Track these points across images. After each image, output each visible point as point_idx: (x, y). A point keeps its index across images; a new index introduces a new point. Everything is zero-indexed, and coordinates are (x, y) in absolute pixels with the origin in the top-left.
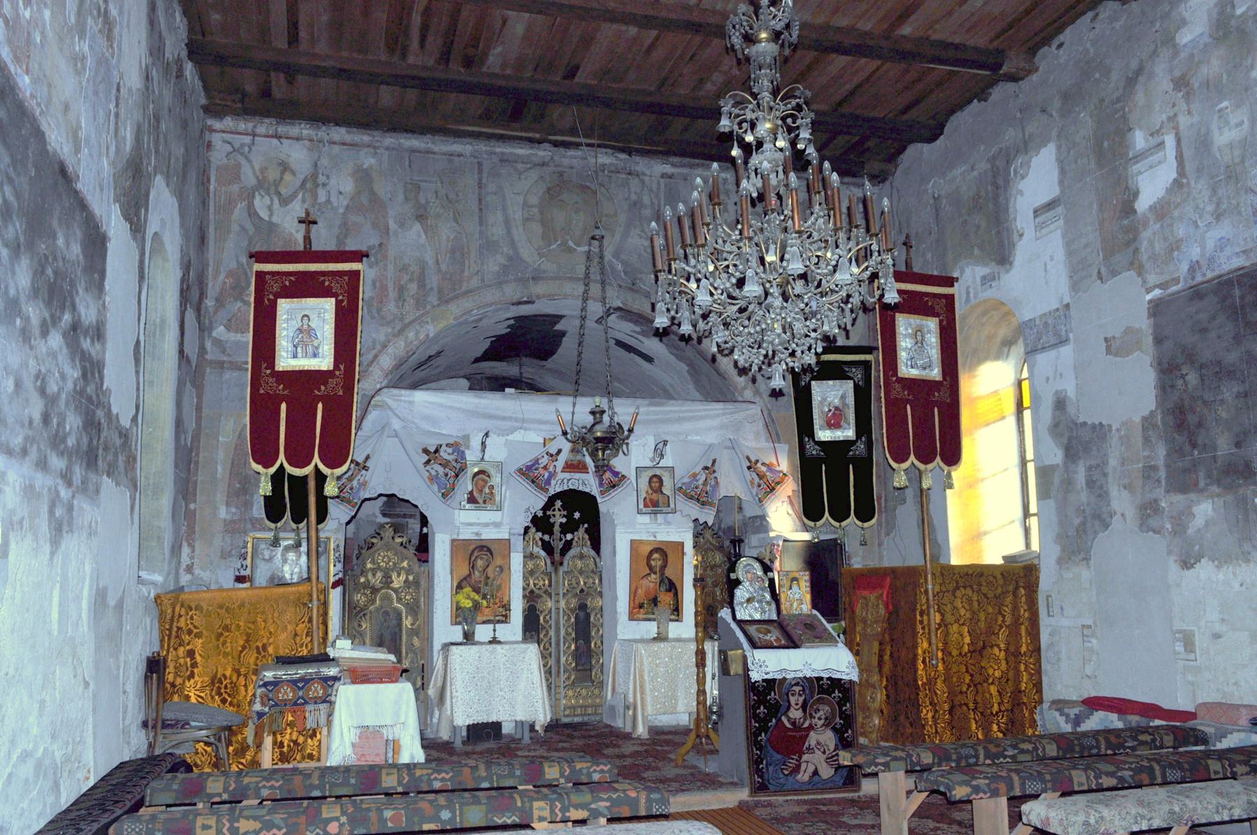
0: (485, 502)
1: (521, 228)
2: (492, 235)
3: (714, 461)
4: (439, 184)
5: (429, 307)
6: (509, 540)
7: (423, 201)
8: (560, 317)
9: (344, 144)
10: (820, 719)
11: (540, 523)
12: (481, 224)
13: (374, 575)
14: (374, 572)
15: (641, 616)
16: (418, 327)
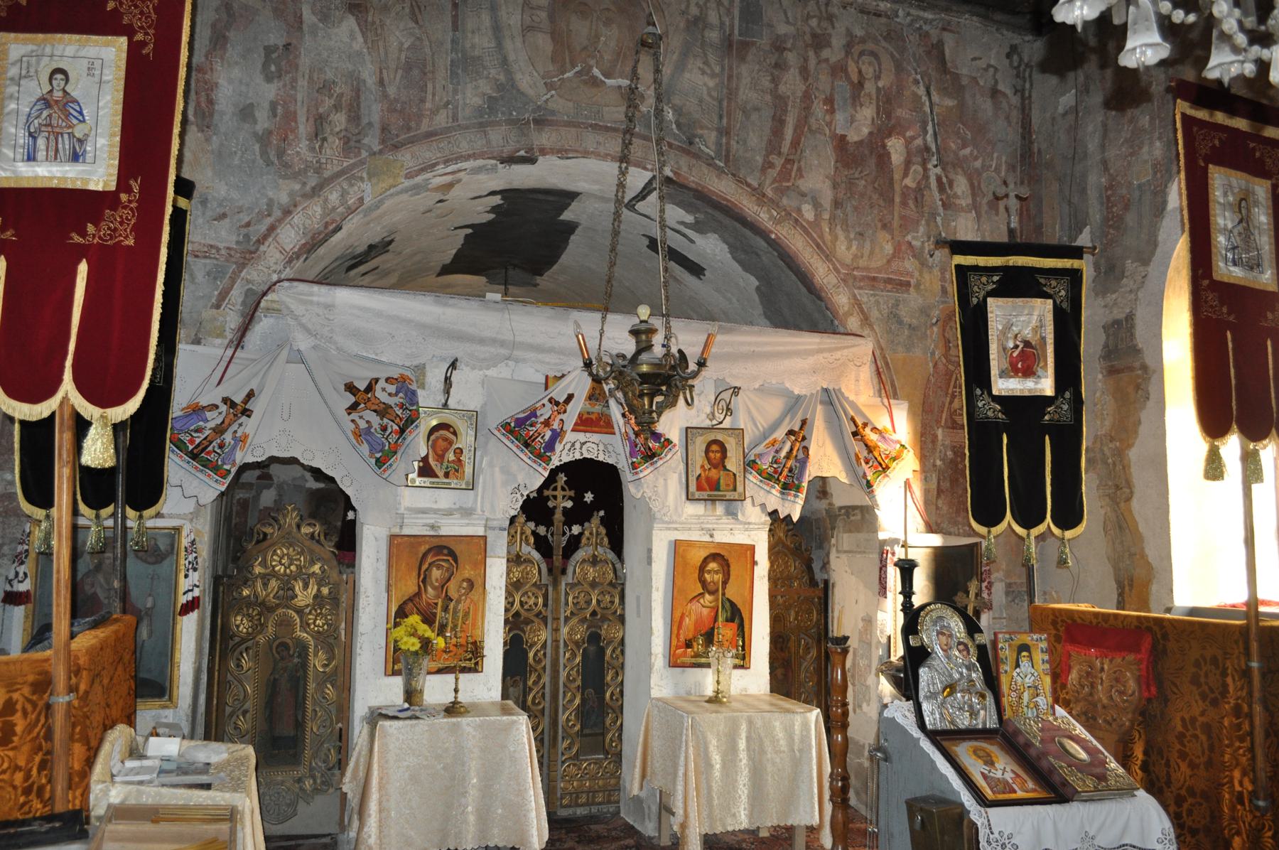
0: (447, 475)
1: (519, 43)
2: (473, 47)
5: (364, 154)
6: (485, 537)
8: (571, 196)
11: (535, 508)
12: (455, 27)
13: (265, 585)
14: (265, 579)
15: (688, 660)
16: (345, 186)
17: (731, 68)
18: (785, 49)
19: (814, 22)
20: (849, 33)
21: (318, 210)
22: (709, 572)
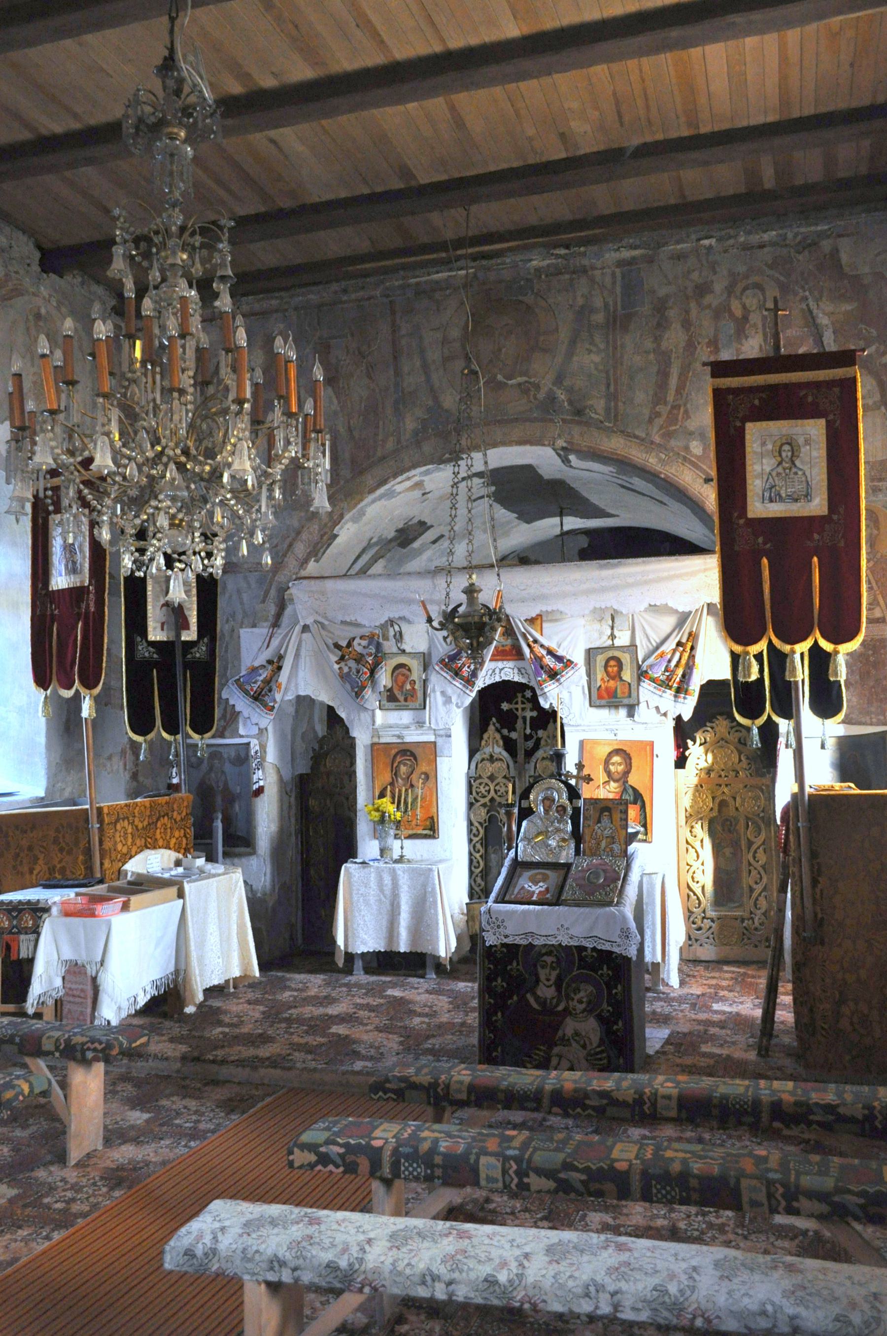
0: (406, 700)
4: (350, 338)
5: (342, 482)
6: (435, 743)
17: (615, 341)
18: (666, 309)
19: (695, 276)
20: (732, 274)
21: (316, 527)
22: (613, 764)
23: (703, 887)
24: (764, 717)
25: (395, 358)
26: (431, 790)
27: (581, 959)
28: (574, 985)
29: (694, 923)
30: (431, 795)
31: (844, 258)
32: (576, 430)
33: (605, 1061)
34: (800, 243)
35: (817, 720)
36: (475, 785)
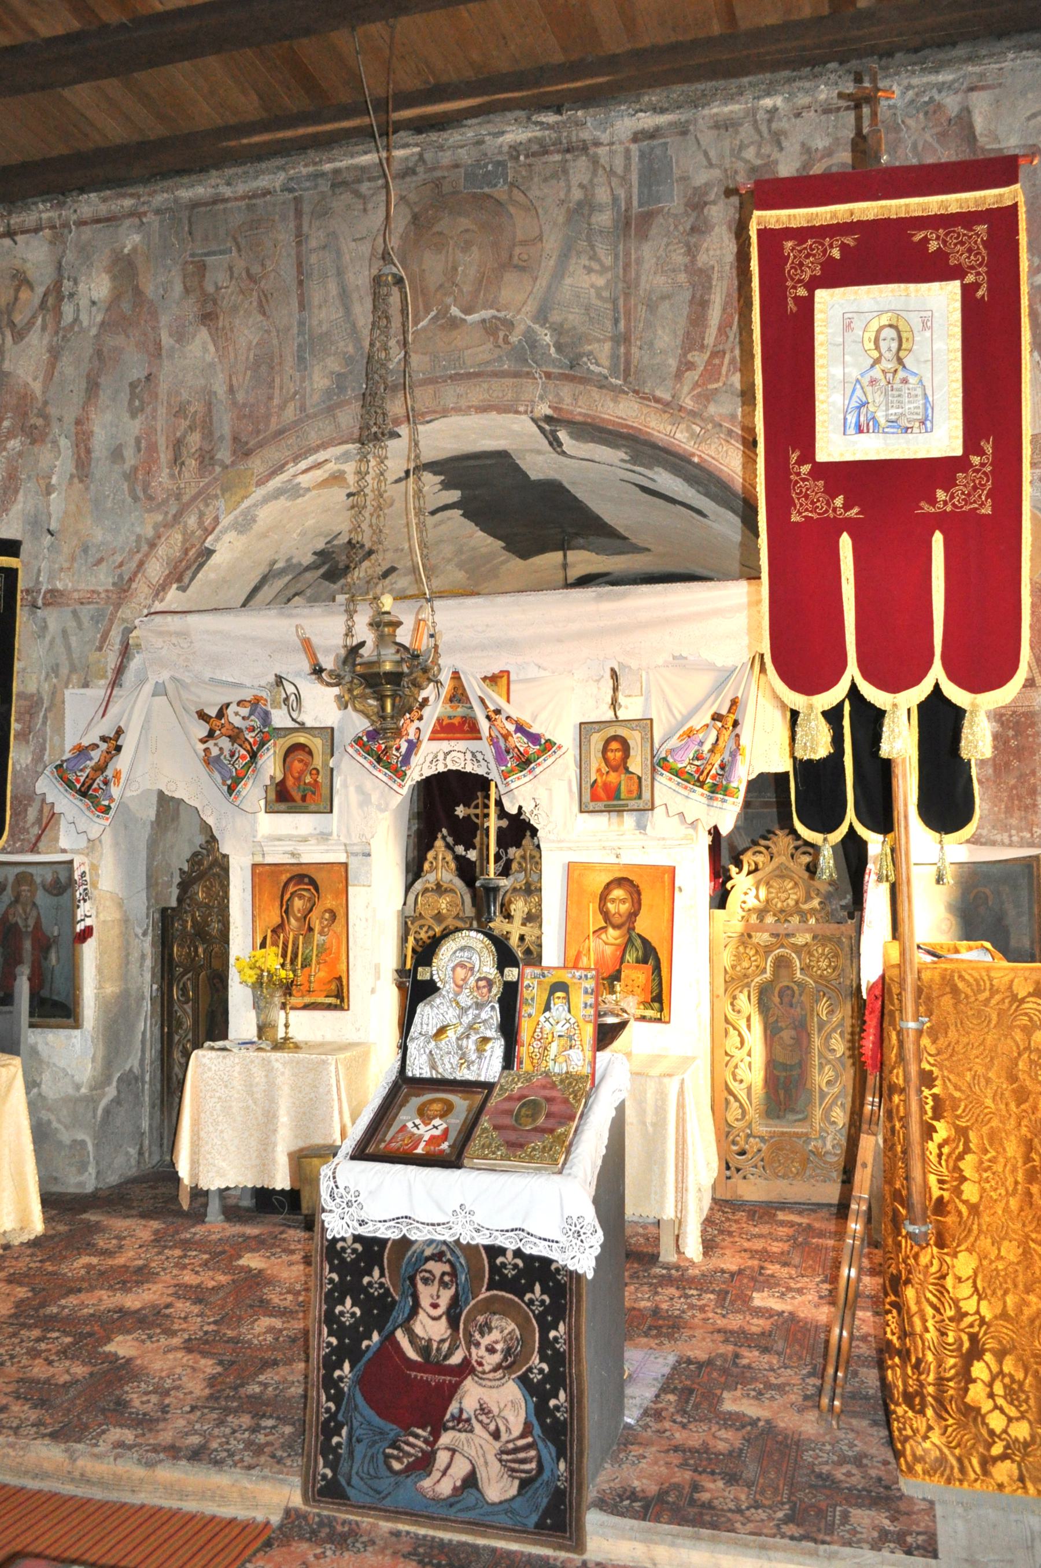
3: (734, 703)
4: (234, 253)
5: (218, 469)
7: (211, 289)
9: (98, 221)
10: (491, 1350)
16: (202, 507)
17: (627, 254)
18: (706, 204)
19: (750, 154)
21: (179, 537)
22: (613, 901)
23: (749, 1088)
24: (843, 829)
25: (301, 283)
26: (338, 938)
27: (495, 1269)
28: (481, 1319)
29: (734, 1143)
30: (339, 947)
31: (979, 123)
32: (566, 391)
33: (533, 1465)
34: (912, 101)
35: (932, 836)
36: (413, 928)
